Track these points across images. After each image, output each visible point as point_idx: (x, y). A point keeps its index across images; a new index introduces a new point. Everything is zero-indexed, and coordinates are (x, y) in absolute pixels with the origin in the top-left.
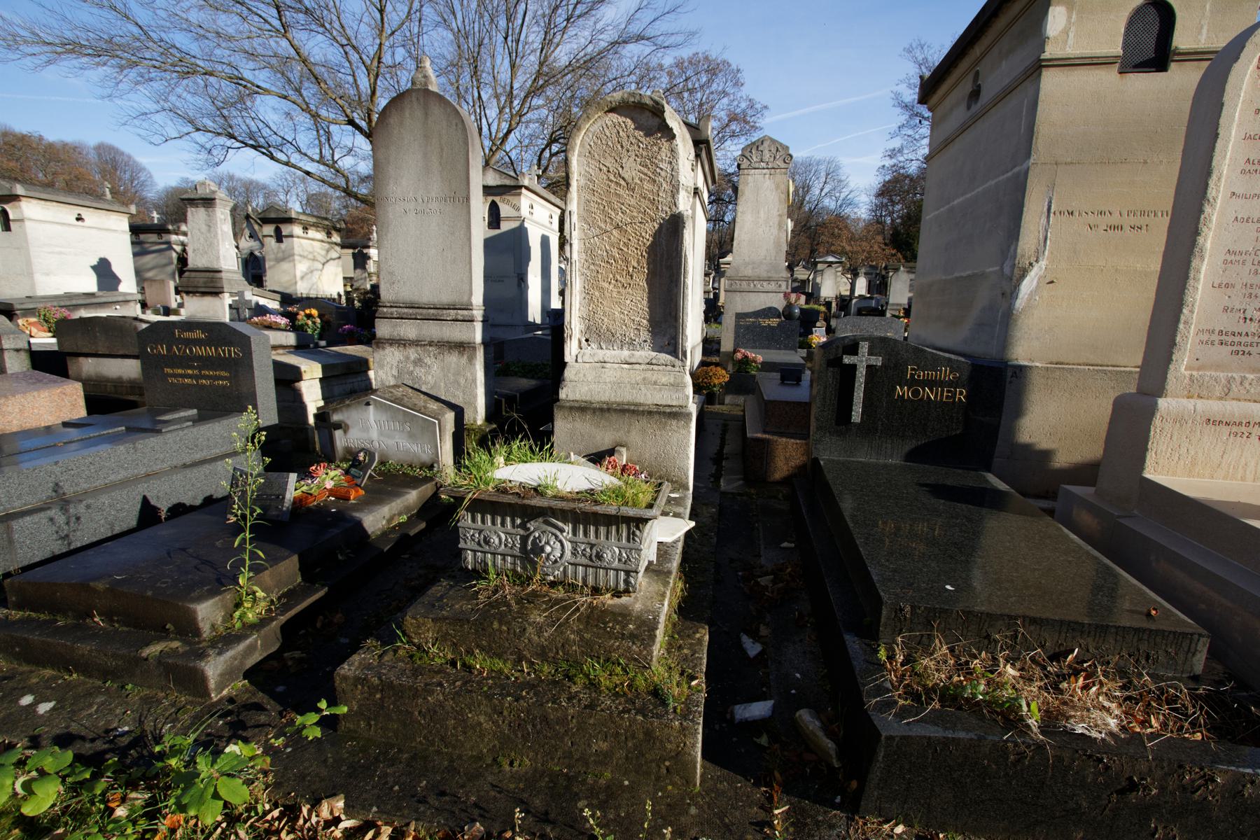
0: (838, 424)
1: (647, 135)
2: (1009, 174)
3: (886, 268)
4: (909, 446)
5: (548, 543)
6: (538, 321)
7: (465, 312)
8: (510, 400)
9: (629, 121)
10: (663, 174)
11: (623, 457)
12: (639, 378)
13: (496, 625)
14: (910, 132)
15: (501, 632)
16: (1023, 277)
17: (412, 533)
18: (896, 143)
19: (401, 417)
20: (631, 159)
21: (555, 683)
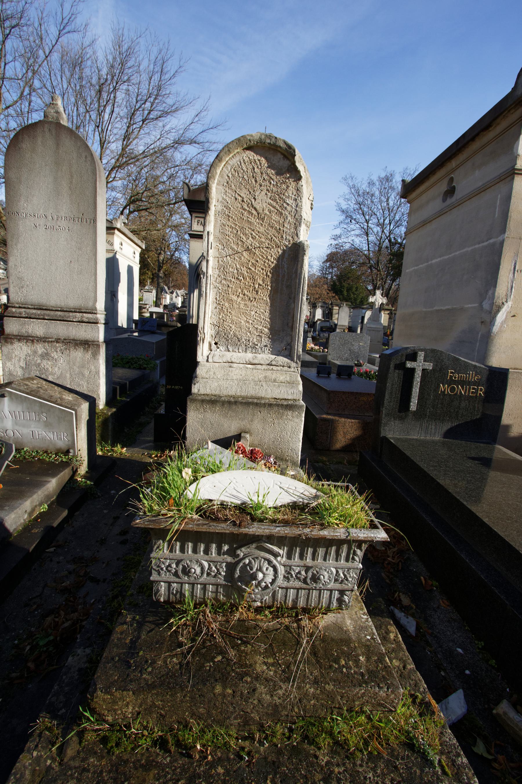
0: (400, 411)
1: (278, 174)
2: (485, 244)
3: (331, 304)
4: (447, 426)
5: (260, 569)
6: (125, 326)
7: (90, 316)
8: (123, 387)
9: (263, 159)
10: (289, 208)
11: (246, 443)
12: (261, 376)
13: (218, 689)
14: (345, 226)
15: (224, 696)
16: (498, 311)
17: (55, 525)
18: (338, 232)
19: (37, 408)
20: (263, 193)
21: (295, 751)
